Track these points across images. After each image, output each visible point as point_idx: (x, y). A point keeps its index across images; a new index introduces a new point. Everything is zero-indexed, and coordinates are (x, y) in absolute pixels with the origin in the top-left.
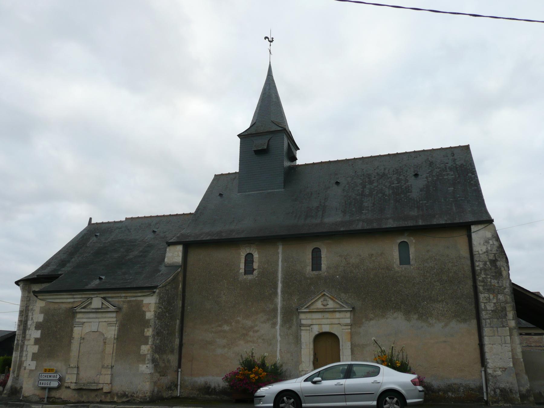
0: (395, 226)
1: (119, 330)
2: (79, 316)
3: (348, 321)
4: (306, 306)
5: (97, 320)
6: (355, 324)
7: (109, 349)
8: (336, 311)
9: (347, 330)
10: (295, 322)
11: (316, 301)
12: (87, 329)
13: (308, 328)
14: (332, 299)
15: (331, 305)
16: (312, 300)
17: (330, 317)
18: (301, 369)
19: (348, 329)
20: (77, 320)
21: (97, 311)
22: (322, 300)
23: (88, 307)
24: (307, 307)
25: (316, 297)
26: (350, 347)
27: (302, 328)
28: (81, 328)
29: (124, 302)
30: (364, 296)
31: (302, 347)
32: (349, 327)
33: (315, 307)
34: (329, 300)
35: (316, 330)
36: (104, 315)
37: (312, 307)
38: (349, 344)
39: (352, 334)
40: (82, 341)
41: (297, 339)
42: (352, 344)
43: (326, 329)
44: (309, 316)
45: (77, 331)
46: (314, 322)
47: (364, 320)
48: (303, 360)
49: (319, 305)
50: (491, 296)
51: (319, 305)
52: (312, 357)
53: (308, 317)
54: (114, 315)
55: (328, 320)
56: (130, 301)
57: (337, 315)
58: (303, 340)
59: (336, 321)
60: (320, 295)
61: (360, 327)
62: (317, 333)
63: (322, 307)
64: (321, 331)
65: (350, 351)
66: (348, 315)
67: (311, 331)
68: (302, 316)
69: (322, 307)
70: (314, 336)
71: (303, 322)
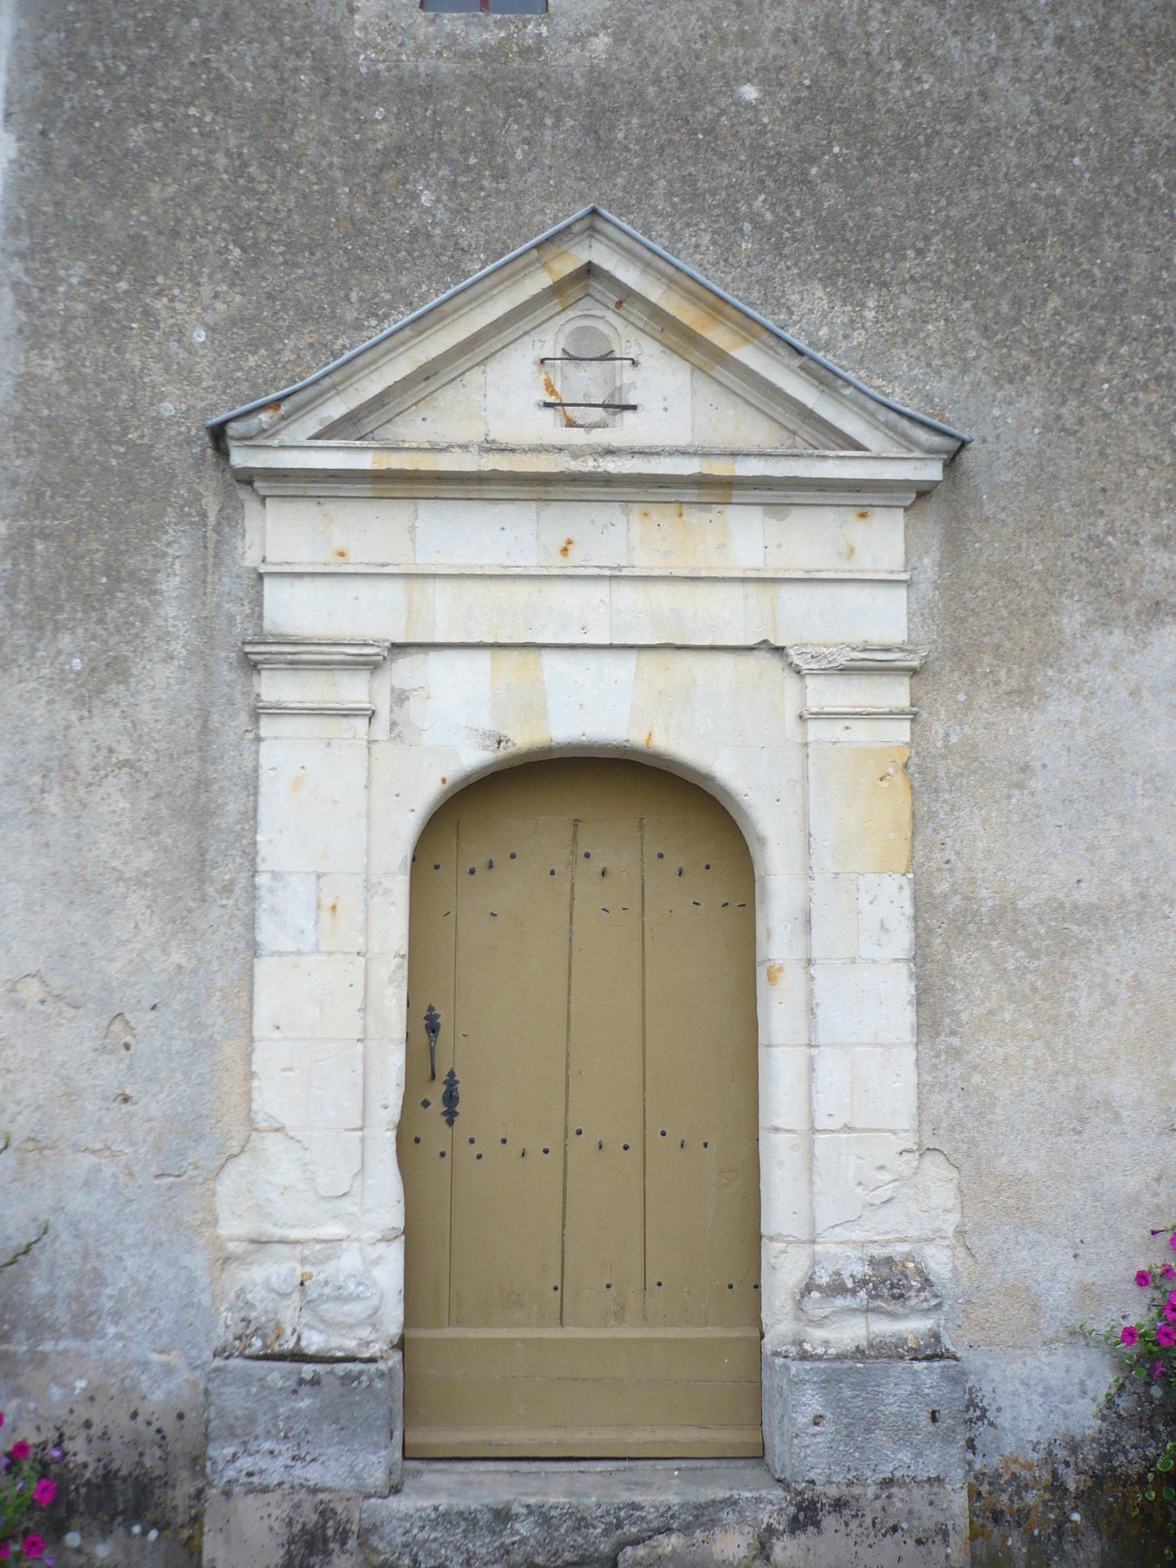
0: (671, 312)
3: (886, 619)
4: (336, 409)
6: (964, 651)
8: (729, 484)
9: (862, 732)
10: (172, 613)
11: (475, 349)
13: (353, 689)
14: (681, 340)
15: (670, 410)
16: (420, 325)
17: (644, 563)
18: (233, 1227)
19: (873, 726)
22: (551, 339)
24: (330, 431)
25: (474, 294)
26: (902, 940)
27: (275, 687)
30: (1074, 335)
31: (267, 933)
32: (898, 694)
33: (472, 432)
34: (649, 351)
35: (461, 722)
37: (415, 428)
38: (892, 900)
39: (921, 775)
41: (205, 836)
42: (923, 904)
43: (590, 708)
44: (371, 532)
46: (445, 613)
47: (1072, 618)
48: (272, 1098)
49: (507, 405)
50: (46, 412)
51: (507, 405)
52: (392, 1062)
53: (361, 556)
55: (627, 594)
57: (746, 538)
58: (281, 841)
59: (731, 616)
60: (540, 281)
61: (1025, 695)
62: (473, 757)
63: (549, 429)
64: (525, 738)
65: (899, 986)
66: (883, 540)
67: (396, 722)
68: (278, 534)
69: (549, 429)
70: (427, 792)
71: (291, 610)
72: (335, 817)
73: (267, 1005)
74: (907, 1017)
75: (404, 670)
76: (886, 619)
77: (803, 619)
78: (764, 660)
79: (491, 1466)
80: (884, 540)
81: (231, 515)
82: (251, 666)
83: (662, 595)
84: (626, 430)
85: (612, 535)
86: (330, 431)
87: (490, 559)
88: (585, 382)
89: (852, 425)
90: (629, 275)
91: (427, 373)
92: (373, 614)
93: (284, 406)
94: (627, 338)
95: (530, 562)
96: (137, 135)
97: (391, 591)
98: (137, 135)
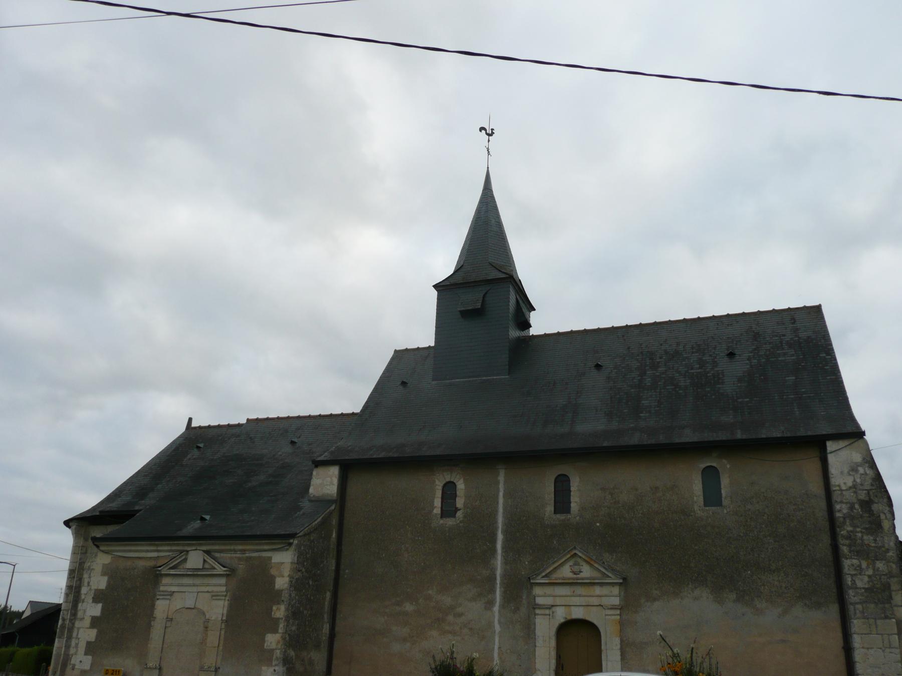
1: (231, 608)
2: (165, 581)
3: (616, 601)
4: (544, 574)
5: (195, 589)
7: (213, 638)
8: (594, 584)
9: (613, 617)
10: (524, 602)
12: (178, 603)
13: (547, 612)
15: (587, 572)
17: (584, 594)
20: (162, 588)
21: (194, 574)
22: (571, 563)
23: (181, 567)
26: (619, 647)
27: (537, 611)
28: (168, 602)
29: (240, 559)
31: (537, 644)
32: (618, 612)
33: (561, 576)
35: (561, 615)
36: (206, 581)
37: (554, 576)
39: (622, 624)
40: (169, 624)
42: (622, 641)
43: (578, 613)
44: (549, 590)
45: (161, 606)
46: (558, 601)
47: (643, 601)
48: (538, 666)
49: (566, 572)
51: (566, 572)
52: (554, 661)
54: (223, 581)
55: (582, 598)
56: (250, 558)
57: (598, 590)
58: (539, 632)
59: (595, 601)
62: (563, 620)
65: (619, 653)
67: (552, 616)
68: (537, 591)
69: (571, 575)
70: (557, 625)
71: (539, 601)
72: (545, 630)
73: (537, 653)
74: (619, 658)
75: (554, 609)
76: (616, 601)
77: (606, 601)
78: (599, 608)
79: (223, 533)
80: (616, 590)
81: (531, 588)
82: (534, 608)
83: (587, 599)
84: (582, 575)
85: (580, 590)
86: (517, 301)
87: (564, 593)
88: (576, 568)
89: (610, 575)
90: (580, 554)
91: (555, 568)
92: (548, 601)
93: (537, 575)
94: (579, 560)
95: (569, 593)
96: (518, 534)
97: (551, 598)
98: (518, 534)
